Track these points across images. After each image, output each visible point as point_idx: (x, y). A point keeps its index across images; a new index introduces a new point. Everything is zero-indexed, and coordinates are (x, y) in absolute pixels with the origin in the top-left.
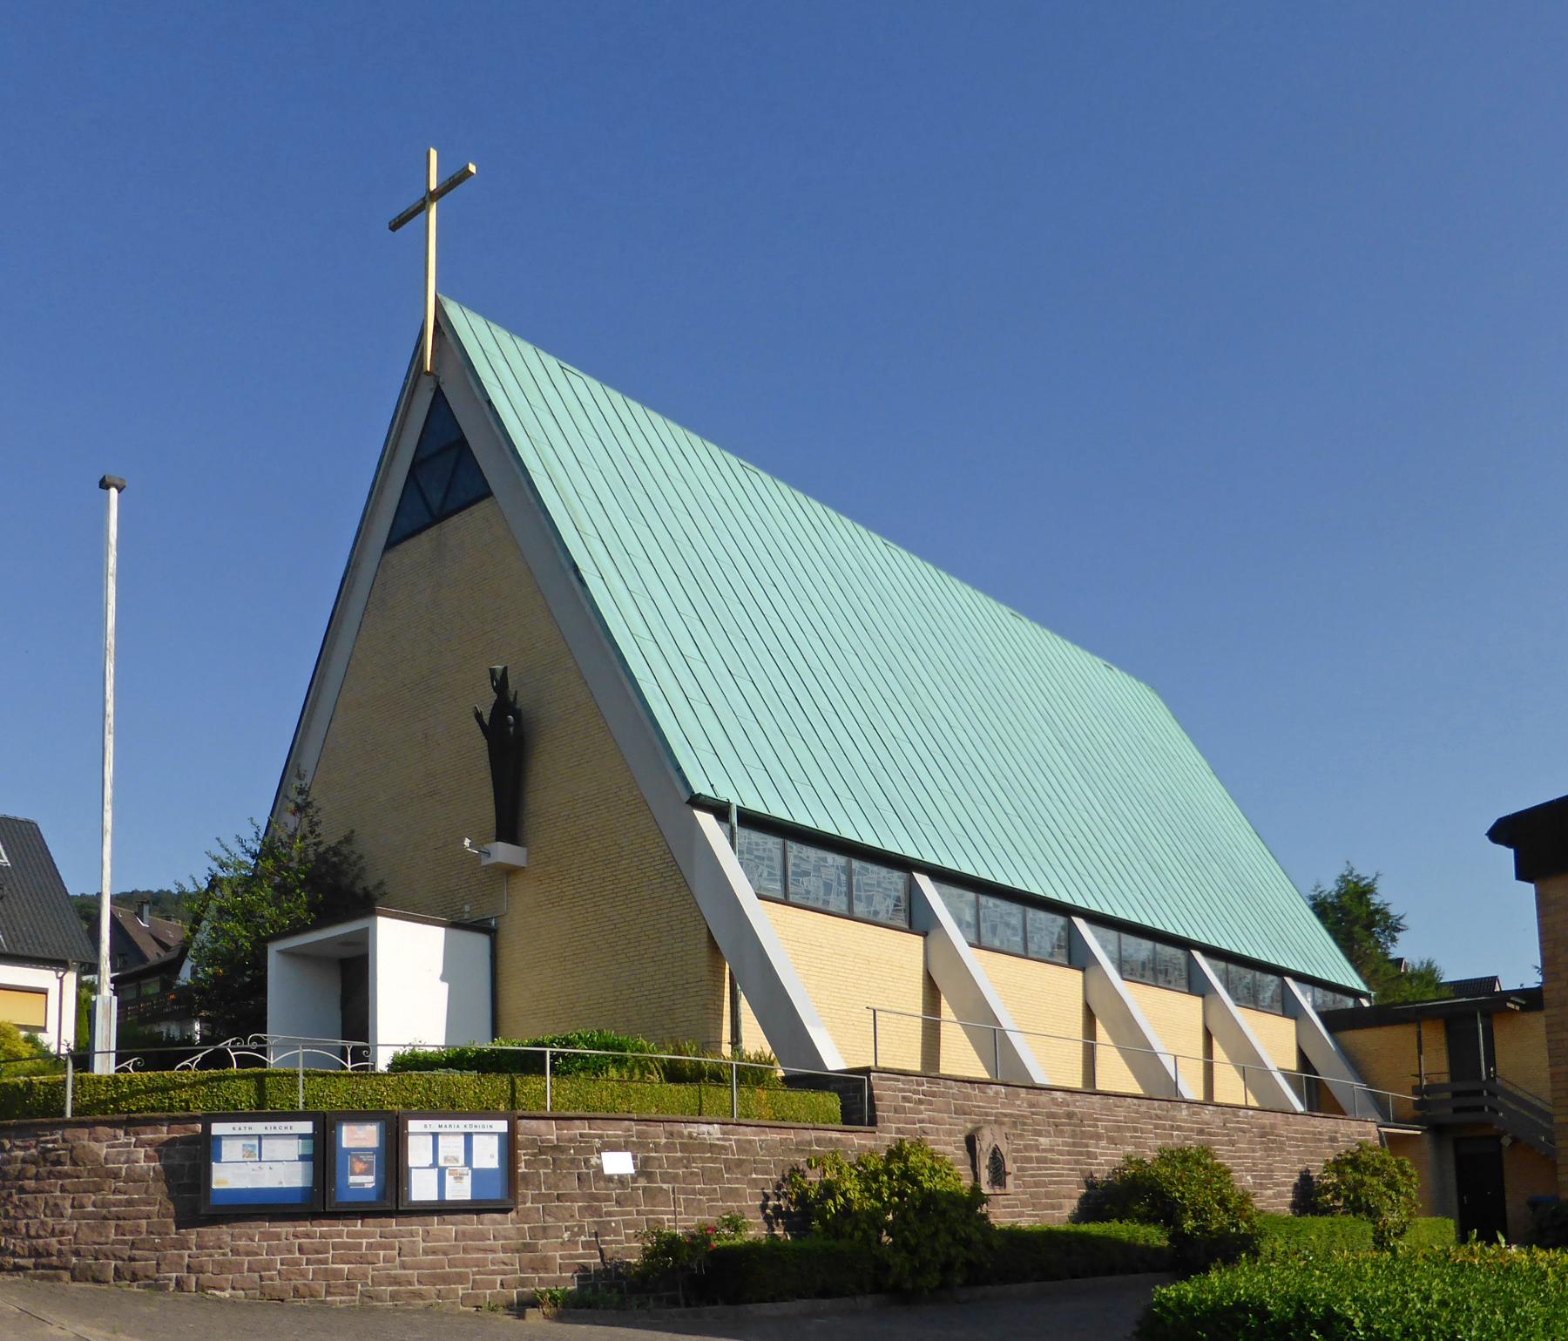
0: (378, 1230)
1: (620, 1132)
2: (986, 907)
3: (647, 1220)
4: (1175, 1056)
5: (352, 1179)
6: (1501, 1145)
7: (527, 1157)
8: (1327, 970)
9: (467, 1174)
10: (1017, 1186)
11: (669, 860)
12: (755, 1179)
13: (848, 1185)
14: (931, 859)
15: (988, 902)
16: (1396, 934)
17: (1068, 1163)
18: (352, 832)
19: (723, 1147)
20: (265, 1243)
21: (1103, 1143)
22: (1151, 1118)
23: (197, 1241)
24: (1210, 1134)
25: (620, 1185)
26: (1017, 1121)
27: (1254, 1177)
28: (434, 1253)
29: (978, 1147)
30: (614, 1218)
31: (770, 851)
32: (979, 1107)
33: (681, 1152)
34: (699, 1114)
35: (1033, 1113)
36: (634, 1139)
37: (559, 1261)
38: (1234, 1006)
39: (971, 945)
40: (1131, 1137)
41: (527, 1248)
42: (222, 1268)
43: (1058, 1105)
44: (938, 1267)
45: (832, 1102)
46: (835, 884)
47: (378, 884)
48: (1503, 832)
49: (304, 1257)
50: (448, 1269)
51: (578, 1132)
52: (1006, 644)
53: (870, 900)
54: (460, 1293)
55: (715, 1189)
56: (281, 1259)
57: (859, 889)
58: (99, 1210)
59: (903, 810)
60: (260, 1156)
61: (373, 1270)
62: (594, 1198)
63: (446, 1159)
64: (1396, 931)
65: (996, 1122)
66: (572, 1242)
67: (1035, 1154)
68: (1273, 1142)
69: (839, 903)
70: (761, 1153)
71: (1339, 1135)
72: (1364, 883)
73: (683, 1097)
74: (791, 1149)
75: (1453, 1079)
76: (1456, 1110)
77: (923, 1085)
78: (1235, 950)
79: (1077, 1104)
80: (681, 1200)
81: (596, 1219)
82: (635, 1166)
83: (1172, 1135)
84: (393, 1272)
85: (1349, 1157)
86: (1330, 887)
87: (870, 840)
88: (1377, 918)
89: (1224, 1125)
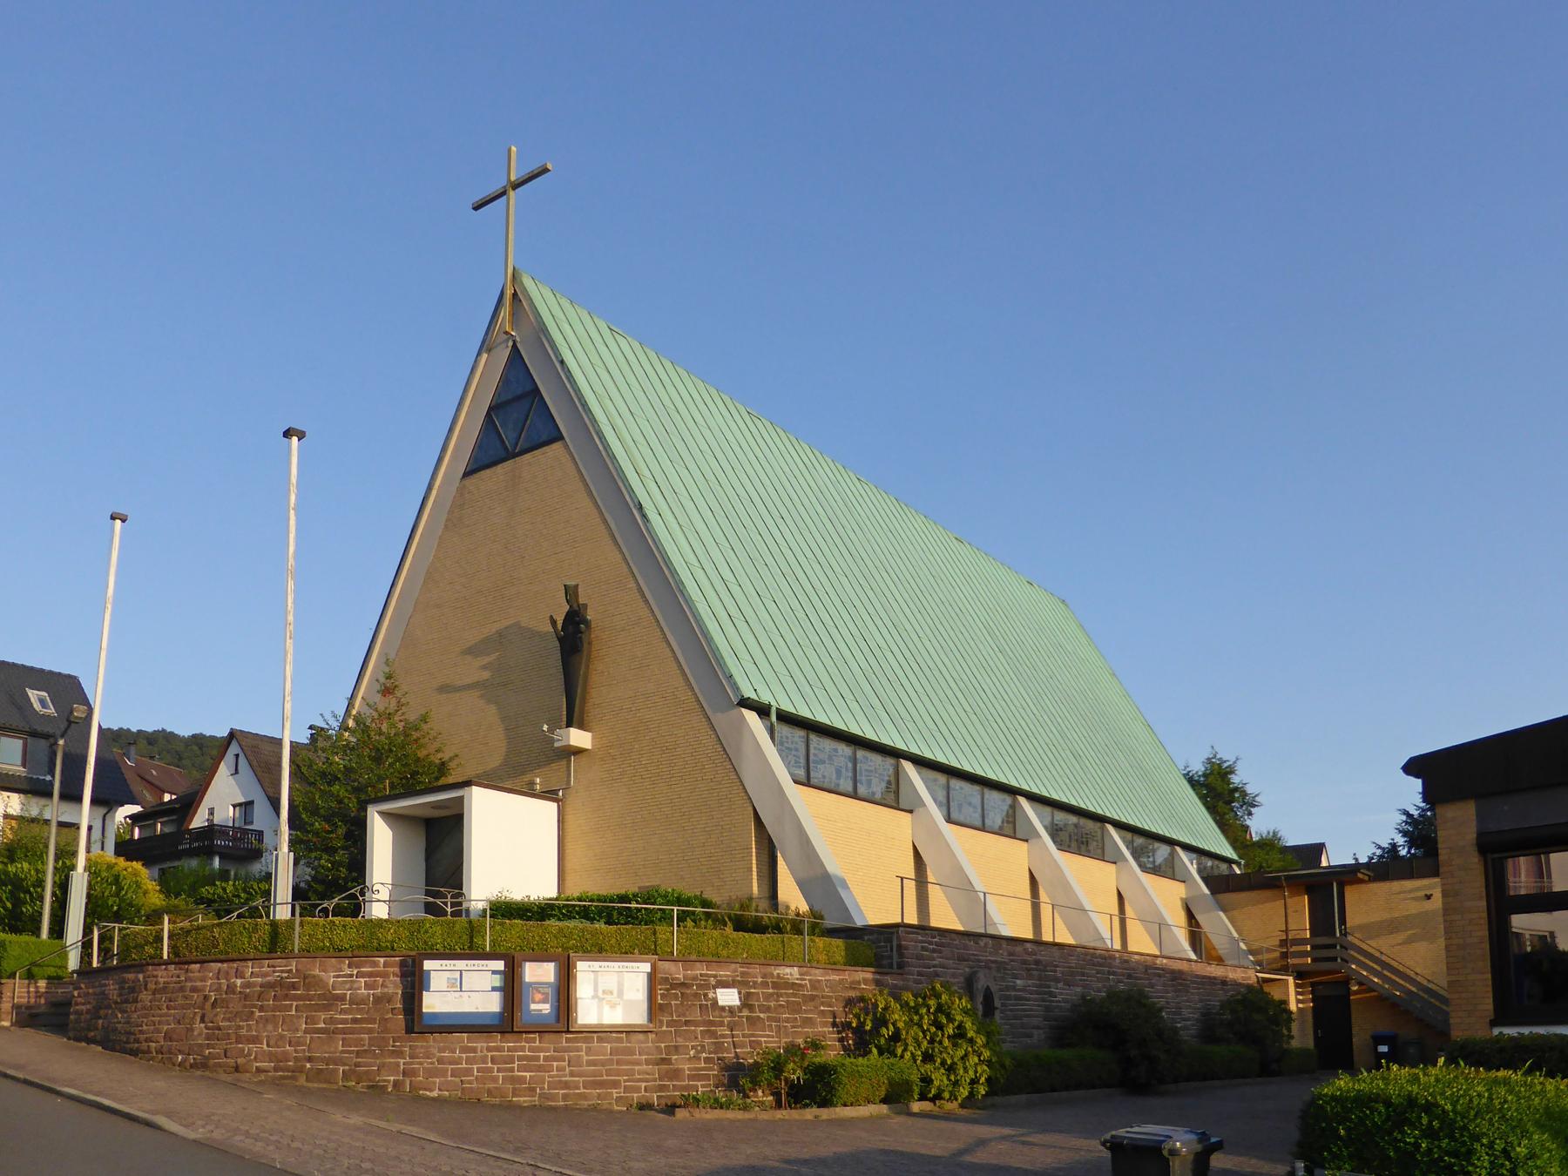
2: (954, 790)
3: (750, 1041)
4: (1111, 915)
5: (533, 1007)
7: (662, 992)
10: (1001, 1018)
13: (897, 1017)
14: (914, 750)
15: (956, 784)
17: (1036, 1000)
19: (800, 985)
20: (464, 1055)
22: (1094, 965)
24: (1136, 978)
26: (1001, 966)
27: (1168, 1013)
28: (595, 1065)
31: (796, 743)
32: (973, 955)
35: (1012, 961)
36: (739, 978)
38: (1141, 873)
39: (796, 782)
40: (1081, 980)
41: (664, 1061)
42: (431, 1073)
46: (843, 770)
48: (1414, 767)
49: (495, 1067)
50: (605, 1078)
53: (869, 783)
54: (615, 1095)
57: (861, 775)
58: (328, 1026)
60: (461, 987)
62: (711, 1023)
63: (604, 992)
64: (1252, 807)
66: (696, 1058)
68: (1181, 984)
69: (1007, 829)
72: (1225, 765)
73: (766, 946)
78: (1161, 832)
82: (740, 998)
84: (564, 1079)
86: (1198, 767)
88: (1237, 795)
89: (1146, 971)
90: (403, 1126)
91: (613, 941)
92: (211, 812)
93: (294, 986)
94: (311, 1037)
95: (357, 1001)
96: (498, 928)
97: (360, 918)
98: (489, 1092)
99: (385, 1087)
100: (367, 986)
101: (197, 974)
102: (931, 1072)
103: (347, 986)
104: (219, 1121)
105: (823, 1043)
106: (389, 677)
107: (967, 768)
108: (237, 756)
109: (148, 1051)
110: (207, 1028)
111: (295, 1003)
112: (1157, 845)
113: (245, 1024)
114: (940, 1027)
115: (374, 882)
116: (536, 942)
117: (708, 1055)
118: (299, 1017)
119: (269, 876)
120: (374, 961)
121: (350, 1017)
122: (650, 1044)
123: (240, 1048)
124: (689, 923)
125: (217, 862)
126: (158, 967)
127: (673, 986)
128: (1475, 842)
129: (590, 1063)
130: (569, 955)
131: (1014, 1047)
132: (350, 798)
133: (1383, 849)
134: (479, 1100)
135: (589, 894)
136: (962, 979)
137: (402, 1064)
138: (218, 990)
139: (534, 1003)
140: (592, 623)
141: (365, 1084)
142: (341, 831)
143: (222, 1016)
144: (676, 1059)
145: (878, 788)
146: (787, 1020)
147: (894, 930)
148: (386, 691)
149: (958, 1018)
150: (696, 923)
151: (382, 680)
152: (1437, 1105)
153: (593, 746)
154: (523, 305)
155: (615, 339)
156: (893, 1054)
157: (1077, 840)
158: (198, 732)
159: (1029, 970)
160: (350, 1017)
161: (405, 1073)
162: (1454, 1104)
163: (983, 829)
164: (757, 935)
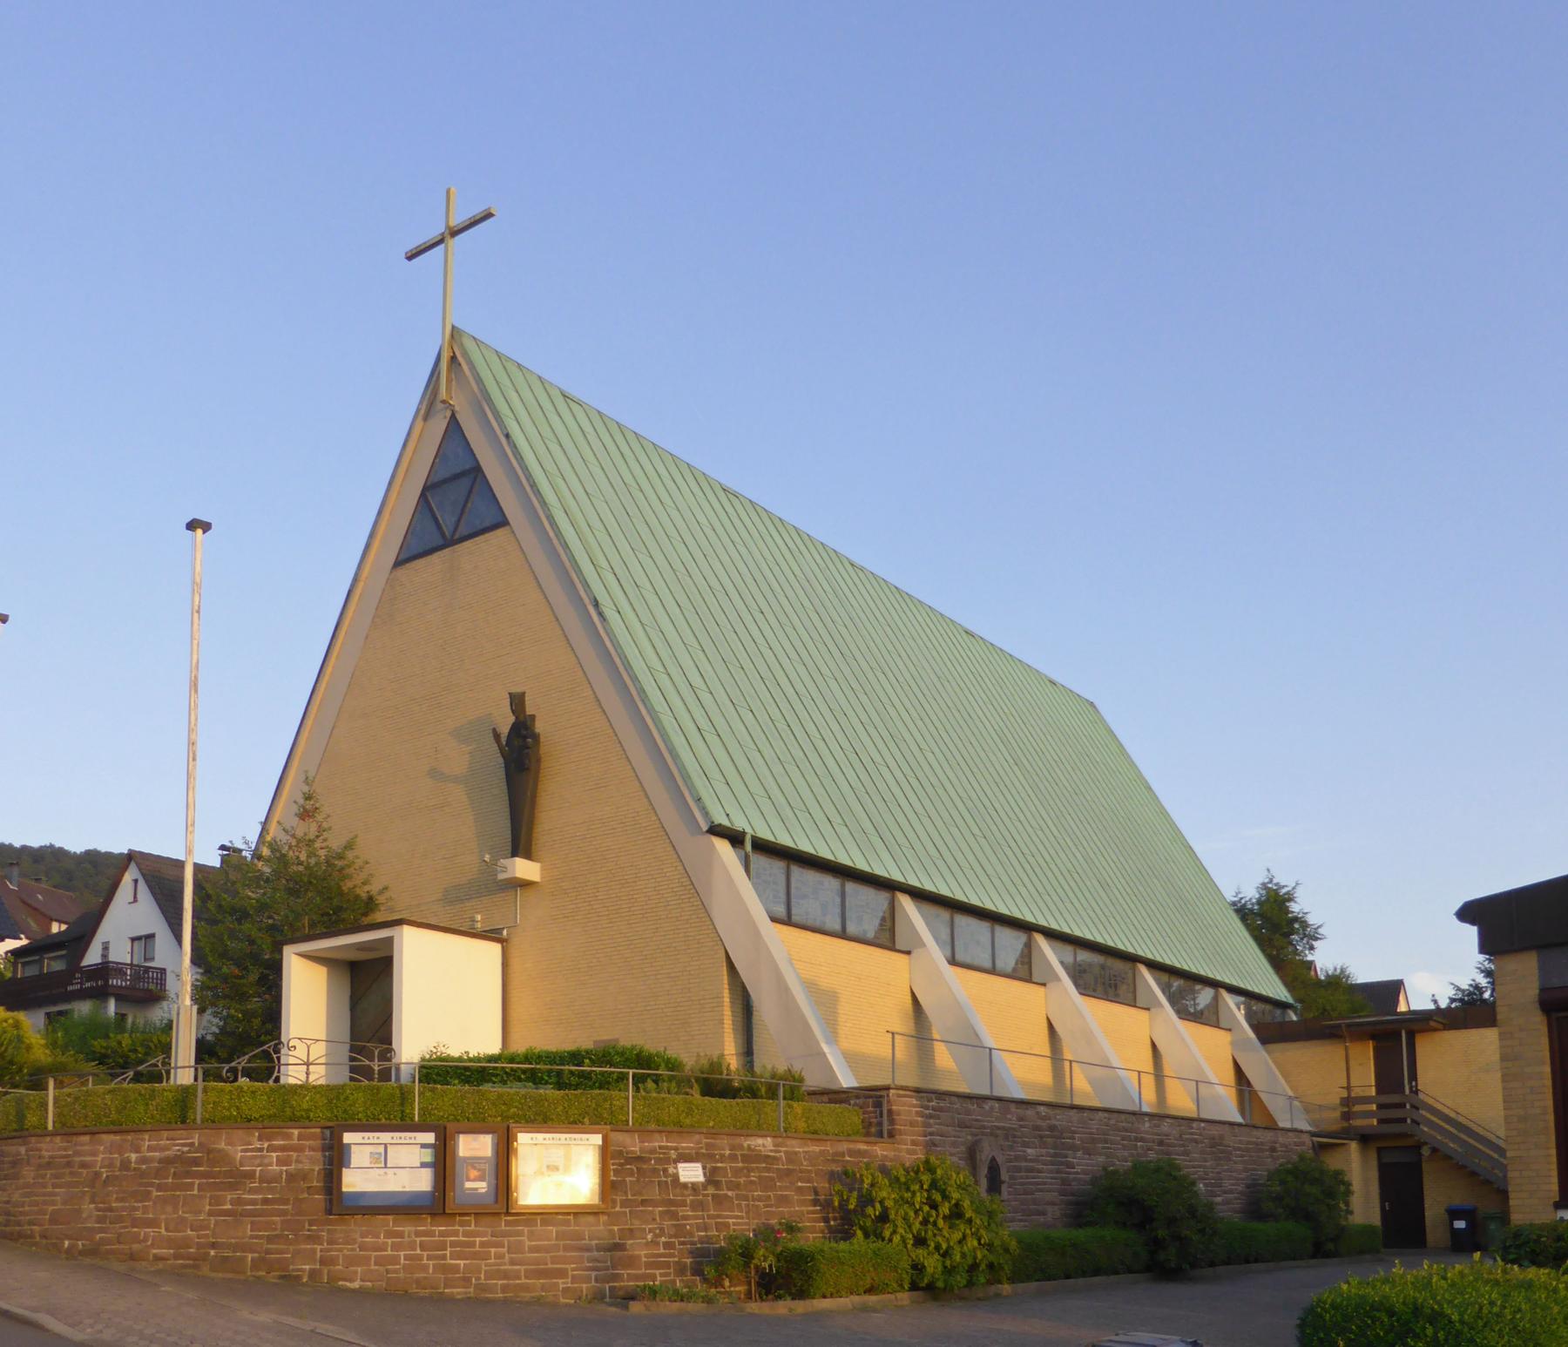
0: (489, 1230)
1: (692, 1145)
3: (716, 1223)
5: (468, 1185)
6: (1420, 1155)
10: (1009, 1193)
13: (884, 1194)
15: (962, 921)
16: (1314, 943)
18: (356, 836)
19: (775, 1158)
21: (1079, 1154)
24: (1169, 1145)
26: (1009, 1134)
27: (1205, 1185)
28: (538, 1251)
29: (978, 1157)
30: (688, 1222)
32: (977, 1120)
33: (743, 1162)
34: (745, 1129)
35: (1021, 1126)
36: (704, 1151)
37: (644, 1259)
38: (1178, 1019)
39: (774, 920)
42: (352, 1261)
43: (1042, 1119)
45: (852, 1117)
47: (384, 889)
48: (1469, 913)
49: (425, 1254)
50: (550, 1266)
51: (657, 1144)
54: (561, 1286)
55: (770, 1196)
56: (405, 1255)
58: (234, 1207)
59: (887, 836)
61: (485, 1266)
62: (672, 1203)
64: (1314, 940)
65: (992, 1134)
66: (655, 1243)
67: (1024, 1164)
70: (805, 1163)
71: (1278, 1145)
72: (1284, 891)
73: (736, 1113)
74: (828, 1160)
75: (1378, 1092)
76: (1381, 1121)
77: (932, 1101)
78: (1121, 947)
79: (1058, 1117)
82: (705, 1174)
83: (1136, 1145)
84: (502, 1268)
86: (1251, 893)
88: (1297, 926)
89: (1181, 1136)
90: (317, 1324)
91: (560, 1109)
92: (106, 947)
93: (196, 1162)
94: (216, 1221)
95: (267, 1179)
96: (428, 1094)
97: (271, 1082)
98: (418, 1281)
99: (298, 1278)
100: (280, 1162)
101: (86, 1148)
102: (924, 1257)
103: (258, 1161)
104: (109, 1319)
105: (800, 1225)
106: (308, 797)
107: (975, 901)
109: (32, 1236)
110: (99, 1210)
111: (197, 1182)
112: (1198, 987)
113: (140, 1205)
114: (934, 1206)
115: (291, 1037)
116: (471, 1111)
117: (667, 1240)
118: (200, 1197)
119: (169, 1026)
120: (286, 1133)
121: (260, 1196)
122: (602, 1227)
123: (135, 1232)
124: (650, 1084)
125: (112, 1007)
126: (41, 1138)
127: (630, 1160)
128: (1537, 999)
129: (533, 1249)
130: (508, 1127)
131: (1026, 1226)
132: (262, 938)
133: (1463, 991)
134: (406, 1292)
135: (536, 1051)
136: (963, 1148)
137: (318, 1250)
138: (111, 1165)
139: (468, 1180)
140: (541, 737)
141: (278, 1273)
142: (253, 977)
143: (115, 1196)
144: (632, 1244)
145: (870, 927)
146: (759, 1199)
147: (883, 1093)
148: (305, 814)
149: (956, 1195)
150: (657, 1084)
151: (301, 801)
152: (1441, 1314)
153: (542, 878)
154: (462, 370)
155: (570, 409)
156: (880, 1237)
157: (1104, 984)
158: (91, 848)
159: (1041, 1137)
160: (260, 1196)
161: (323, 1262)
162: (1461, 1315)
163: (993, 971)
164: (725, 1100)
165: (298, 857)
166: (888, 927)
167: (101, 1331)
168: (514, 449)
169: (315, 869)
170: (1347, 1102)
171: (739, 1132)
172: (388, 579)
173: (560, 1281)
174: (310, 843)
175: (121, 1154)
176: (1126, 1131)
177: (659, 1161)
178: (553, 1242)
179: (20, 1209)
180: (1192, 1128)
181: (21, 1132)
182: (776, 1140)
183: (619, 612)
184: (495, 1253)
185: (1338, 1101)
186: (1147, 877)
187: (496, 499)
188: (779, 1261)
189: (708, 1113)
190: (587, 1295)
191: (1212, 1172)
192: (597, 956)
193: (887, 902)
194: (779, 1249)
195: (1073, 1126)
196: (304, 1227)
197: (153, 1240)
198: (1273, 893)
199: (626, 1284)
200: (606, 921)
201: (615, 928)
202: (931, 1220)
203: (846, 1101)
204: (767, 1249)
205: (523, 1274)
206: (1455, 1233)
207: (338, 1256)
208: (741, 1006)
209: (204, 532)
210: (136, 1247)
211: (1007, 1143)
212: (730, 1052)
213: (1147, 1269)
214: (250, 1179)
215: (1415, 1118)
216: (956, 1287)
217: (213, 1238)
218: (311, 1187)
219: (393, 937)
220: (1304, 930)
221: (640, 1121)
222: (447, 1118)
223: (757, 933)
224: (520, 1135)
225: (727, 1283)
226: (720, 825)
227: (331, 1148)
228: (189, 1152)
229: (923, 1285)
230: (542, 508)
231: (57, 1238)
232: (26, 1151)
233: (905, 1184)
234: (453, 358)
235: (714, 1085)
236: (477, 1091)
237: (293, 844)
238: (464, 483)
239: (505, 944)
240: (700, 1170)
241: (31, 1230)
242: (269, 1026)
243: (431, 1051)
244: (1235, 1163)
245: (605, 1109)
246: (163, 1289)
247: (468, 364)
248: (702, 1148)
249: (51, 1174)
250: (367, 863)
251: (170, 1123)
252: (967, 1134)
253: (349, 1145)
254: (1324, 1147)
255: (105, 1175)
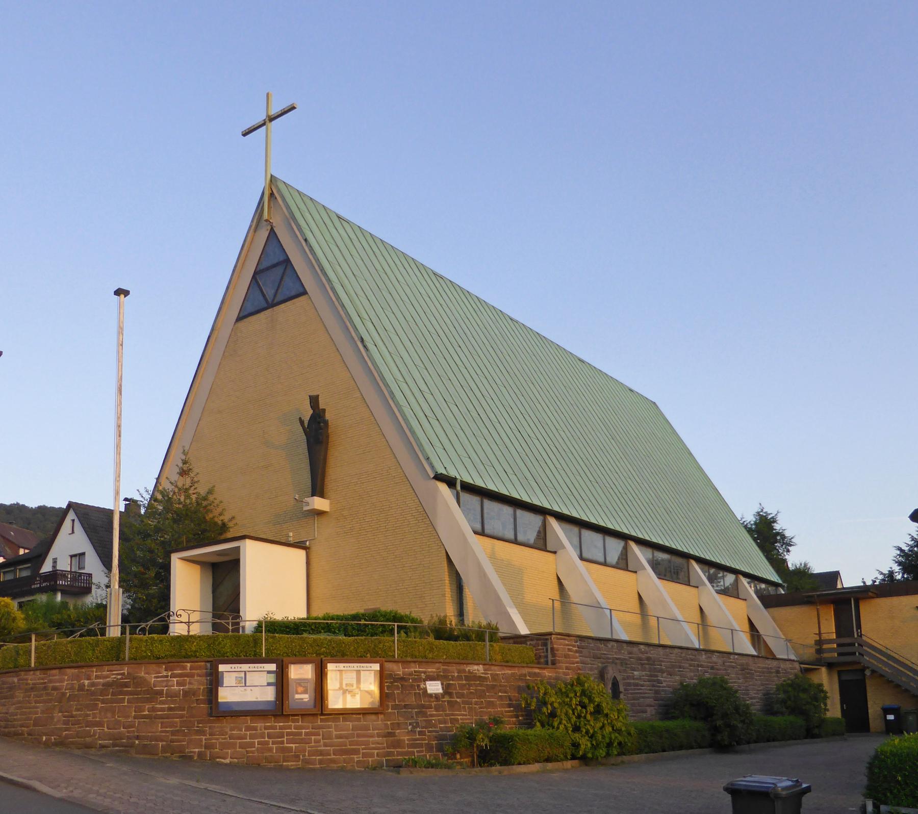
0: (310, 725)
4: (610, 610)
5: (297, 696)
6: (864, 675)
8: (698, 549)
9: (358, 694)
11: (421, 510)
12: (501, 696)
13: (553, 699)
16: (789, 548)
18: (214, 486)
19: (485, 678)
23: (209, 732)
25: (436, 700)
26: (623, 662)
28: (341, 738)
33: (465, 681)
34: (465, 660)
35: (631, 658)
36: (442, 674)
37: (407, 742)
39: (476, 533)
42: (224, 746)
44: (605, 745)
49: (271, 740)
50: (349, 747)
52: (578, 378)
54: (356, 760)
59: (539, 481)
60: (245, 683)
62: (423, 706)
65: (613, 663)
67: (632, 681)
70: (503, 681)
71: (780, 669)
72: (770, 517)
74: (517, 679)
76: (840, 654)
77: (577, 642)
78: (680, 548)
79: (652, 652)
80: (467, 708)
81: (424, 719)
82: (443, 688)
83: (698, 669)
84: (319, 748)
85: (790, 682)
87: (526, 499)
88: (778, 538)
89: (724, 664)
90: (208, 785)
92: (55, 561)
93: (126, 685)
95: (172, 695)
96: (270, 640)
98: (266, 758)
100: (178, 684)
101: (57, 677)
103: (164, 684)
108: (73, 521)
111: (127, 697)
113: (91, 712)
117: (421, 730)
120: (182, 665)
121: (166, 706)
123: (88, 730)
125: (59, 597)
127: (396, 680)
134: (259, 765)
136: (596, 672)
138: (72, 688)
139: (297, 693)
140: (329, 422)
142: (152, 573)
144: (398, 733)
145: (531, 537)
147: (548, 637)
148: (183, 473)
149: (597, 700)
150: (407, 634)
151: (181, 465)
153: (331, 509)
159: (642, 664)
160: (166, 706)
163: (605, 564)
165: (179, 499)
166: (542, 537)
167: (72, 791)
168: (310, 248)
169: (189, 506)
170: (819, 643)
171: (462, 661)
172: (233, 329)
173: (355, 756)
174: (186, 490)
175: (79, 681)
176: (692, 660)
177: (414, 680)
178: (351, 732)
179: (15, 717)
180: (731, 659)
181: (17, 669)
182: (485, 666)
183: (376, 345)
184: (314, 739)
185: (813, 642)
186: (692, 507)
187: (299, 278)
188: (490, 741)
189: (443, 651)
190: (372, 765)
191: (744, 686)
192: (366, 556)
193: (541, 521)
194: (491, 734)
195: (660, 658)
196: (194, 724)
197: (99, 735)
198: (763, 518)
199: (396, 757)
200: (370, 535)
201: (377, 539)
202: (583, 715)
203: (525, 643)
204: (484, 734)
205: (332, 752)
206: (888, 722)
207: (216, 743)
208: (455, 586)
209: (125, 297)
210: (88, 739)
211: (622, 668)
212: (450, 612)
213: (710, 746)
214: (160, 695)
215: (861, 652)
216: (599, 757)
217: (137, 733)
218: (198, 700)
219: (239, 546)
220: (783, 540)
221: (401, 655)
222: (282, 655)
223: (465, 539)
224: (329, 665)
225: (458, 756)
226: (442, 473)
227: (211, 674)
228: (122, 679)
229: (579, 756)
230: (328, 284)
231: (38, 735)
232: (18, 681)
233: (565, 693)
234: (272, 194)
235: (441, 632)
236: (301, 638)
237: (176, 491)
238: (279, 270)
239: (308, 550)
240: (440, 685)
241: (22, 730)
242: (163, 603)
243: (265, 617)
244: (756, 680)
245: (380, 648)
246: (108, 765)
247: (281, 197)
248: (440, 672)
249: (34, 695)
250: (221, 502)
251: (108, 661)
252: (598, 663)
253: (222, 672)
254: (807, 671)
255: (68, 694)
